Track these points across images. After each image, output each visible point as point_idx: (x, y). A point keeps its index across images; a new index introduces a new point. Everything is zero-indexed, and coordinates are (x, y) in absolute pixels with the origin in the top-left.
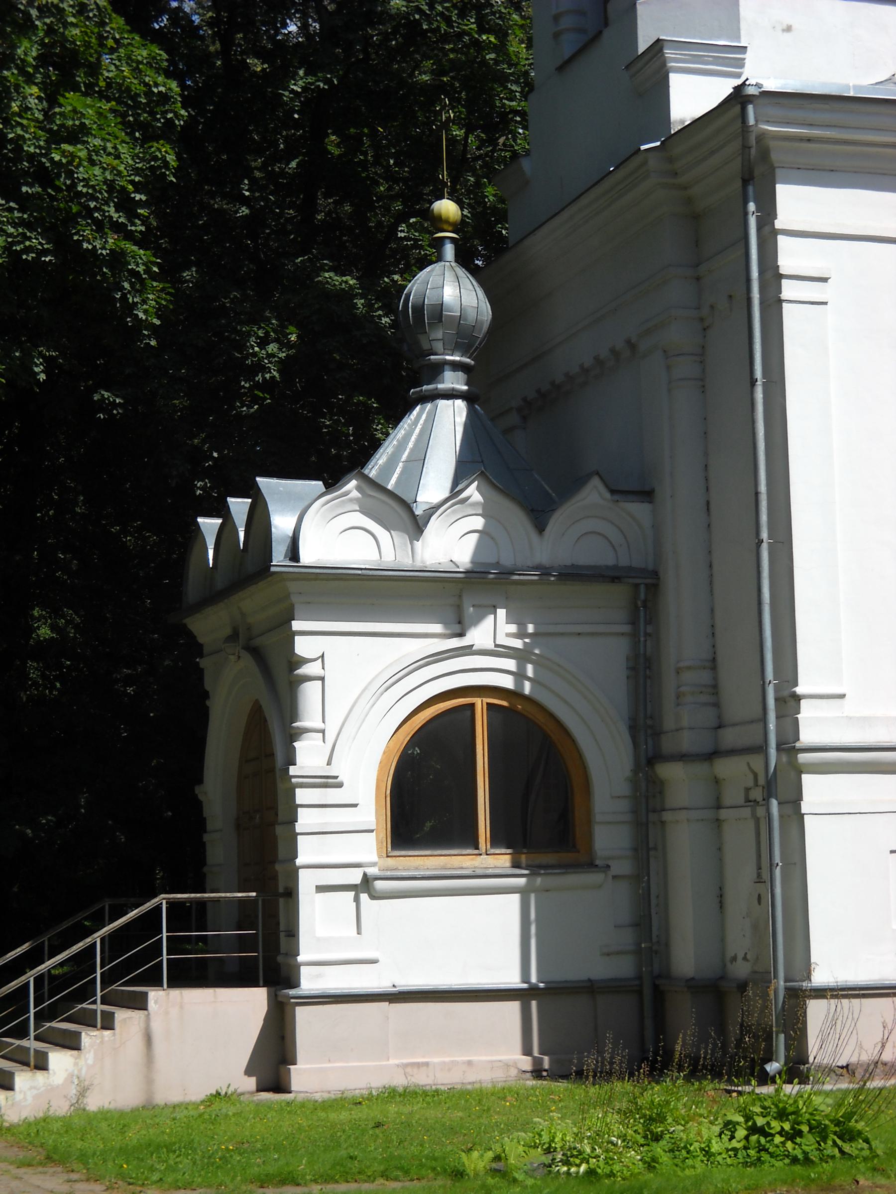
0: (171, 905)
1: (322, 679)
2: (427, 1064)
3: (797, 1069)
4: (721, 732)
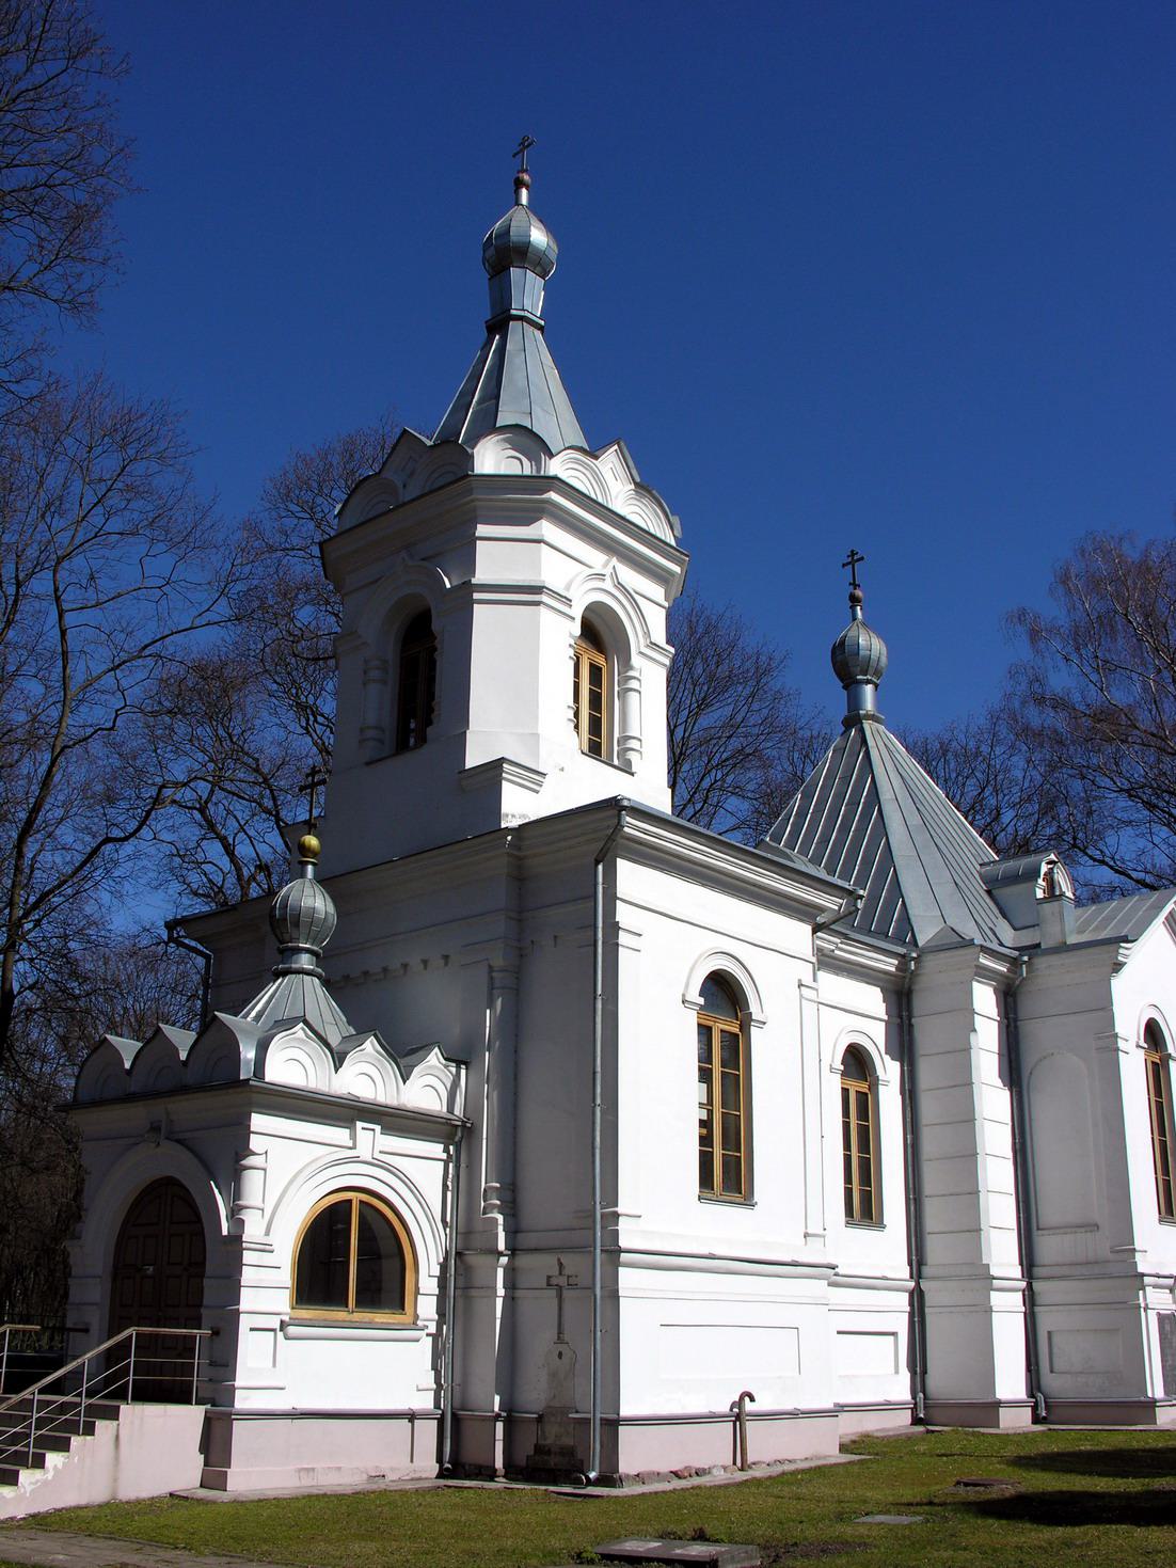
0: (14, 1333)
1: (265, 1170)
2: (313, 1469)
3: (609, 1478)
4: (520, 1236)
